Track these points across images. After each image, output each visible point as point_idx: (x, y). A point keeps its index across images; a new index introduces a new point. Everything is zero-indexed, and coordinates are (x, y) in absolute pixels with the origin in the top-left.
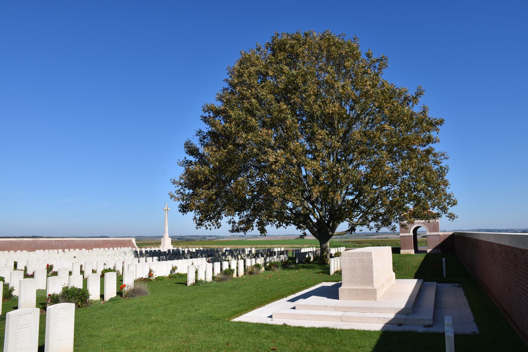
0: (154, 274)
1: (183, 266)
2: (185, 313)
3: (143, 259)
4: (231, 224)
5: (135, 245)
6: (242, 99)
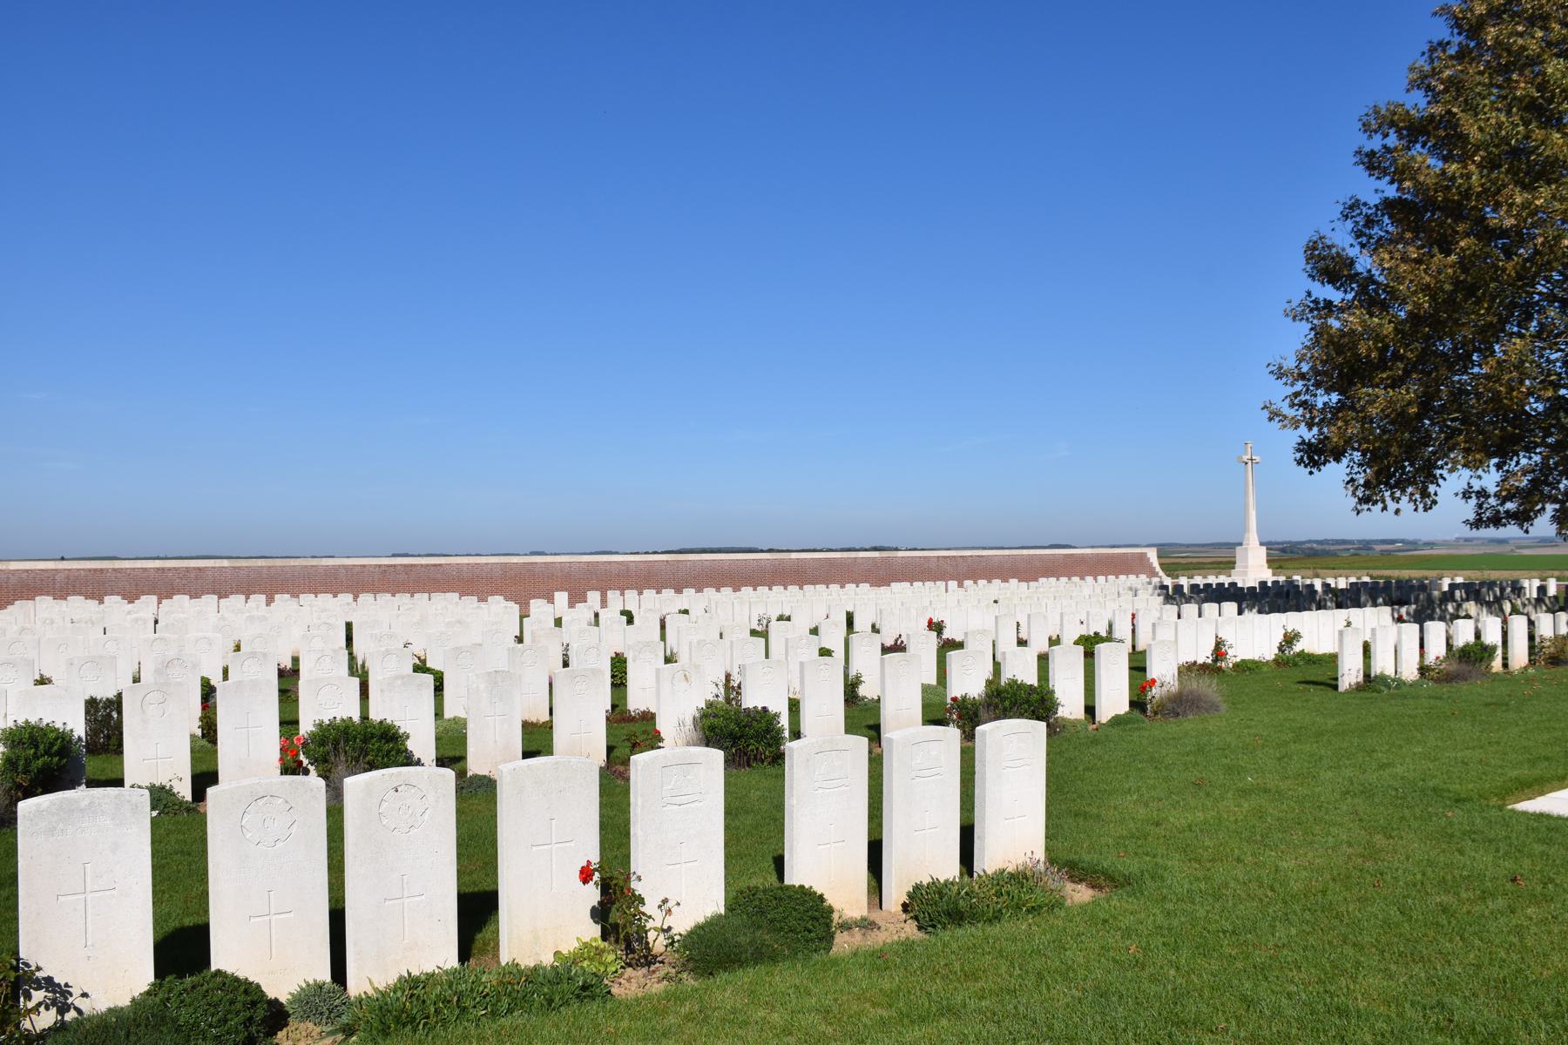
0: (1231, 652)
1: (1318, 631)
2: (1348, 773)
3: (1190, 609)
4: (1473, 501)
5: (1158, 569)
6: (1505, 70)
